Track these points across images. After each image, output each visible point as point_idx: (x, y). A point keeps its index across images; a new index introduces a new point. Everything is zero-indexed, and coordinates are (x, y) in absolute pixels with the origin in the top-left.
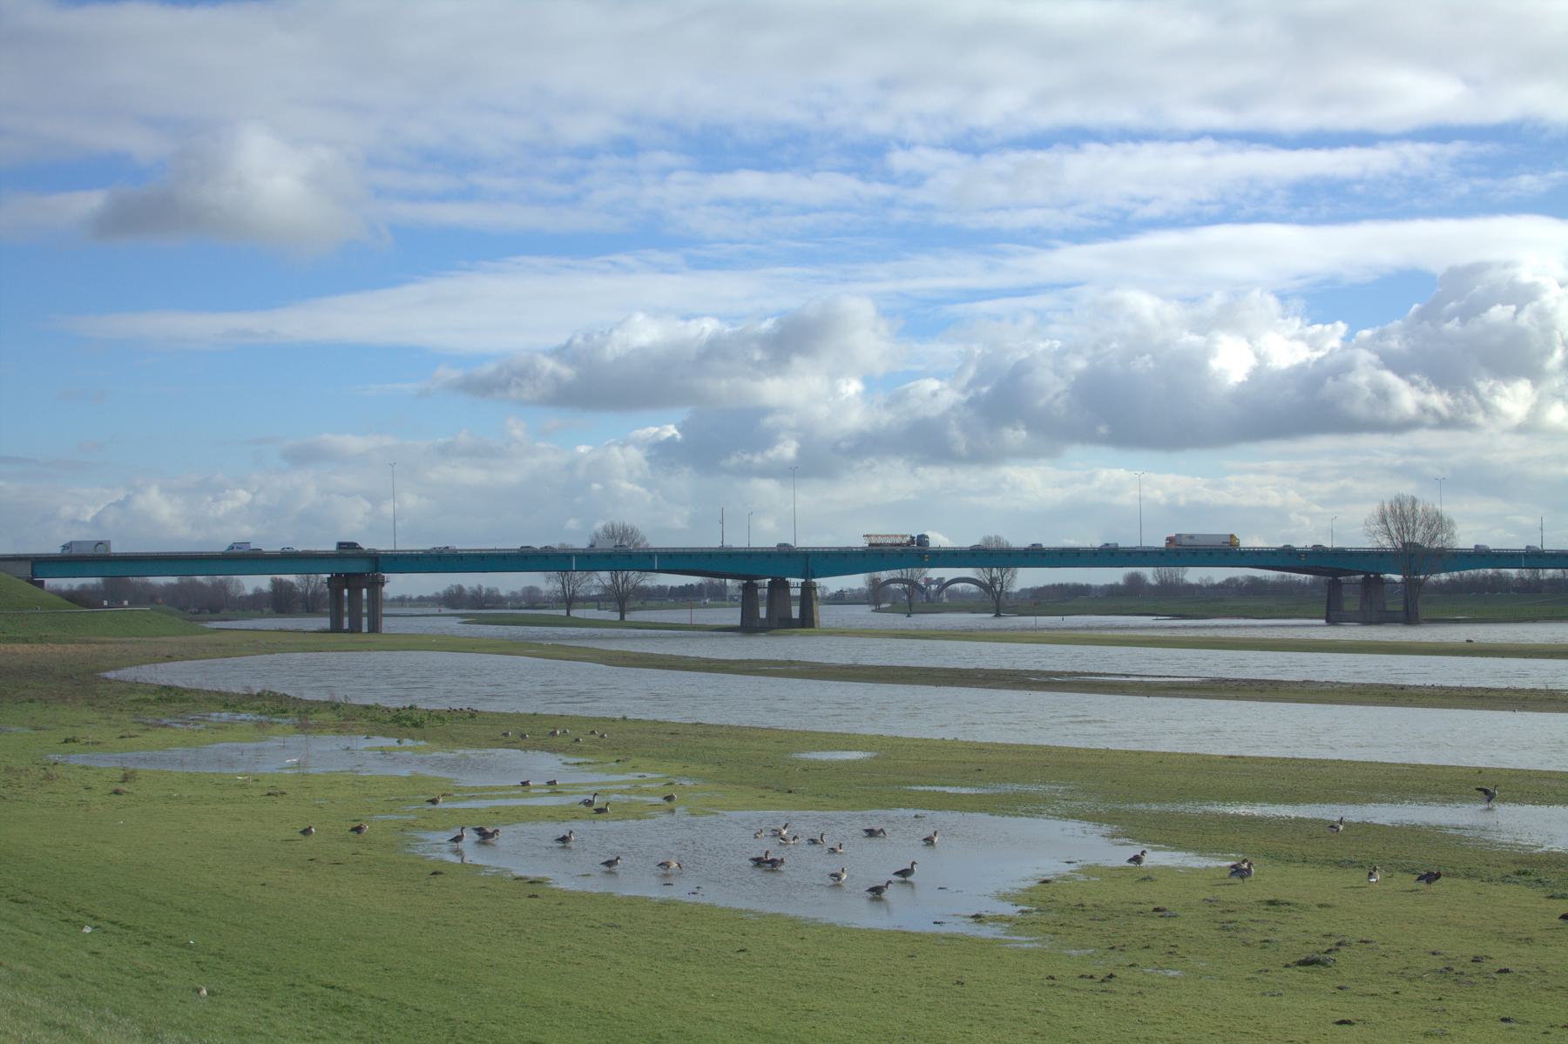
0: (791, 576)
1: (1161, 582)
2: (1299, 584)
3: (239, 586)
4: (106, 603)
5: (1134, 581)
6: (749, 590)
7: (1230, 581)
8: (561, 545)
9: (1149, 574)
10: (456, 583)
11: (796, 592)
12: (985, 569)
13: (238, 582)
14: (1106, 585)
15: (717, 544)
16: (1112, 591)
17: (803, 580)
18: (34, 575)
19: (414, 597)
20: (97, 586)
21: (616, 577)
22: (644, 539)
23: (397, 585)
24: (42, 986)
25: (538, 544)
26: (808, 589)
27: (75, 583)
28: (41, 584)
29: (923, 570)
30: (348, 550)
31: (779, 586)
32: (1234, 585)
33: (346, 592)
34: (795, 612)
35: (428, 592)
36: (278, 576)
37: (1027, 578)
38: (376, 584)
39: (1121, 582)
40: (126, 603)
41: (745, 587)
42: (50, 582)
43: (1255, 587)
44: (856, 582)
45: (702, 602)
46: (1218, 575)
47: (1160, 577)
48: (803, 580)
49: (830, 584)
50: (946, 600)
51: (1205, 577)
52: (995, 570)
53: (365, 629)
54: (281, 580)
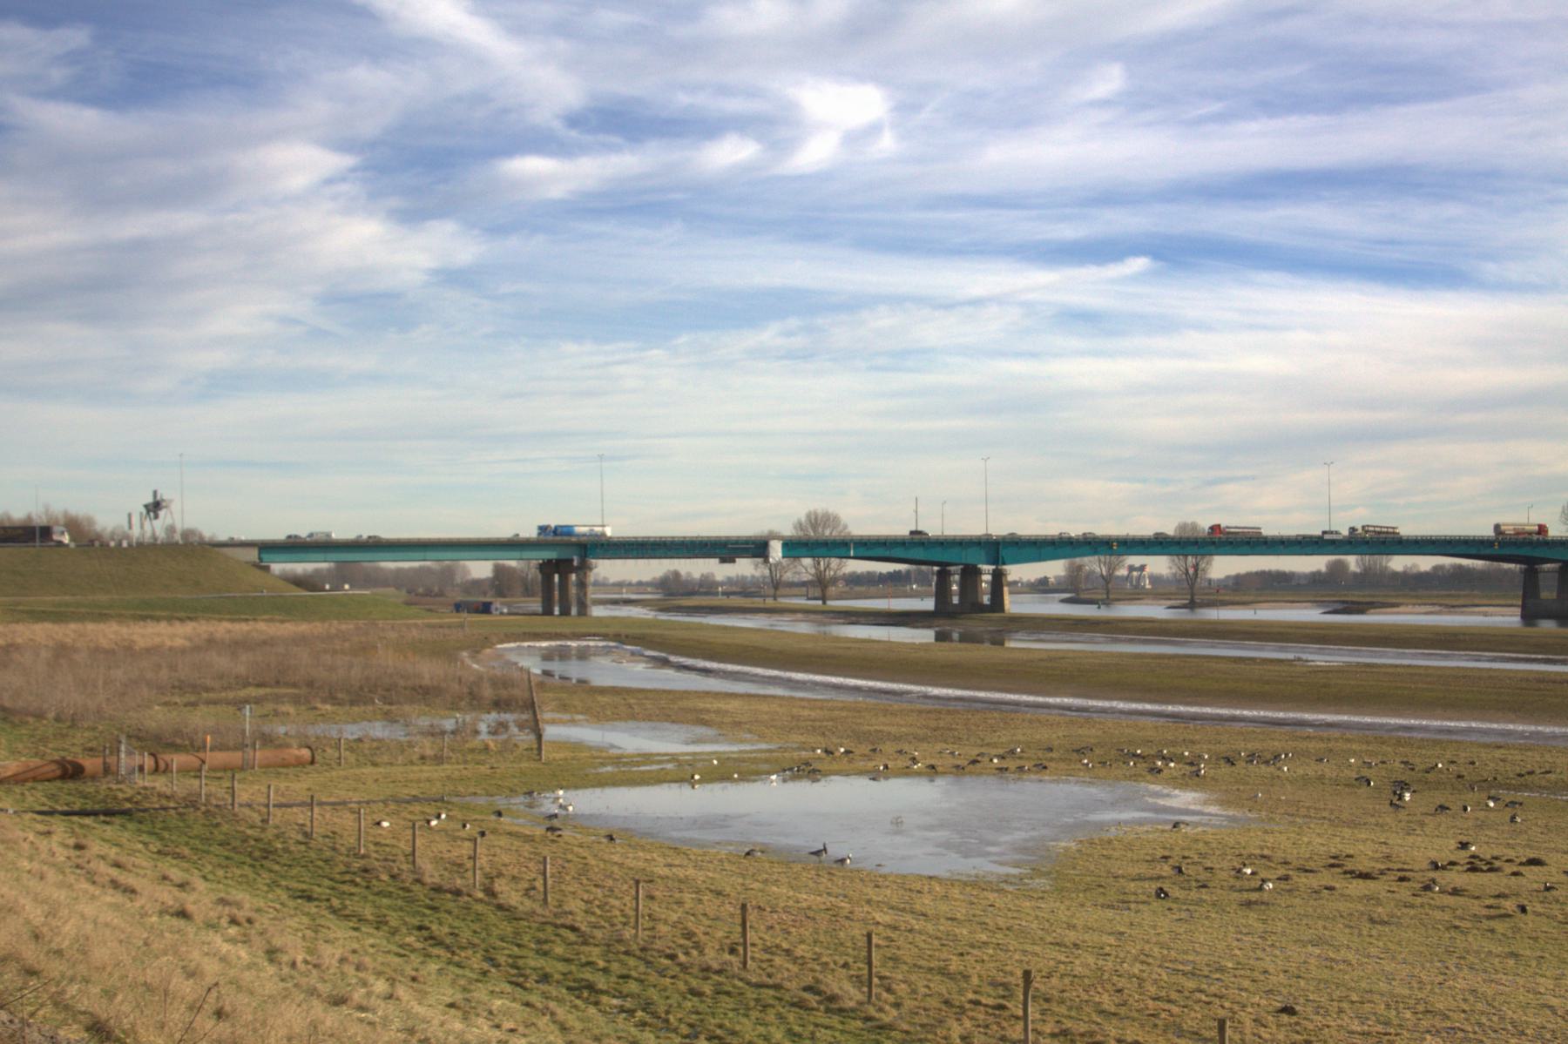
0: (983, 563)
1: (1365, 570)
2: (1507, 572)
3: (466, 571)
4: (327, 587)
5: (1337, 570)
6: (943, 577)
7: (1436, 568)
8: (1183, 527)
9: (1353, 562)
10: (672, 568)
11: (987, 577)
12: (1181, 557)
13: (464, 567)
14: (1228, 577)
15: (939, 533)
16: (1315, 580)
17: (994, 567)
18: (261, 560)
19: (635, 580)
20: (329, 570)
21: (819, 563)
22: (845, 527)
23: (606, 570)
24: (905, 890)
25: (303, 533)
26: (998, 577)
27: (301, 568)
28: (267, 569)
29: (1122, 558)
30: (554, 537)
31: (971, 573)
32: (1440, 573)
33: (556, 578)
34: (986, 599)
35: (646, 578)
36: (501, 562)
37: (1223, 567)
38: (584, 568)
39: (1323, 569)
40: (347, 587)
41: (1526, 572)
42: (277, 568)
43: (1460, 575)
44: (1054, 569)
45: (908, 588)
46: (1425, 563)
47: (1364, 564)
48: (994, 567)
49: (1019, 572)
50: (1148, 586)
51: (1409, 565)
52: (1190, 558)
53: (557, 611)
54: (503, 566)
